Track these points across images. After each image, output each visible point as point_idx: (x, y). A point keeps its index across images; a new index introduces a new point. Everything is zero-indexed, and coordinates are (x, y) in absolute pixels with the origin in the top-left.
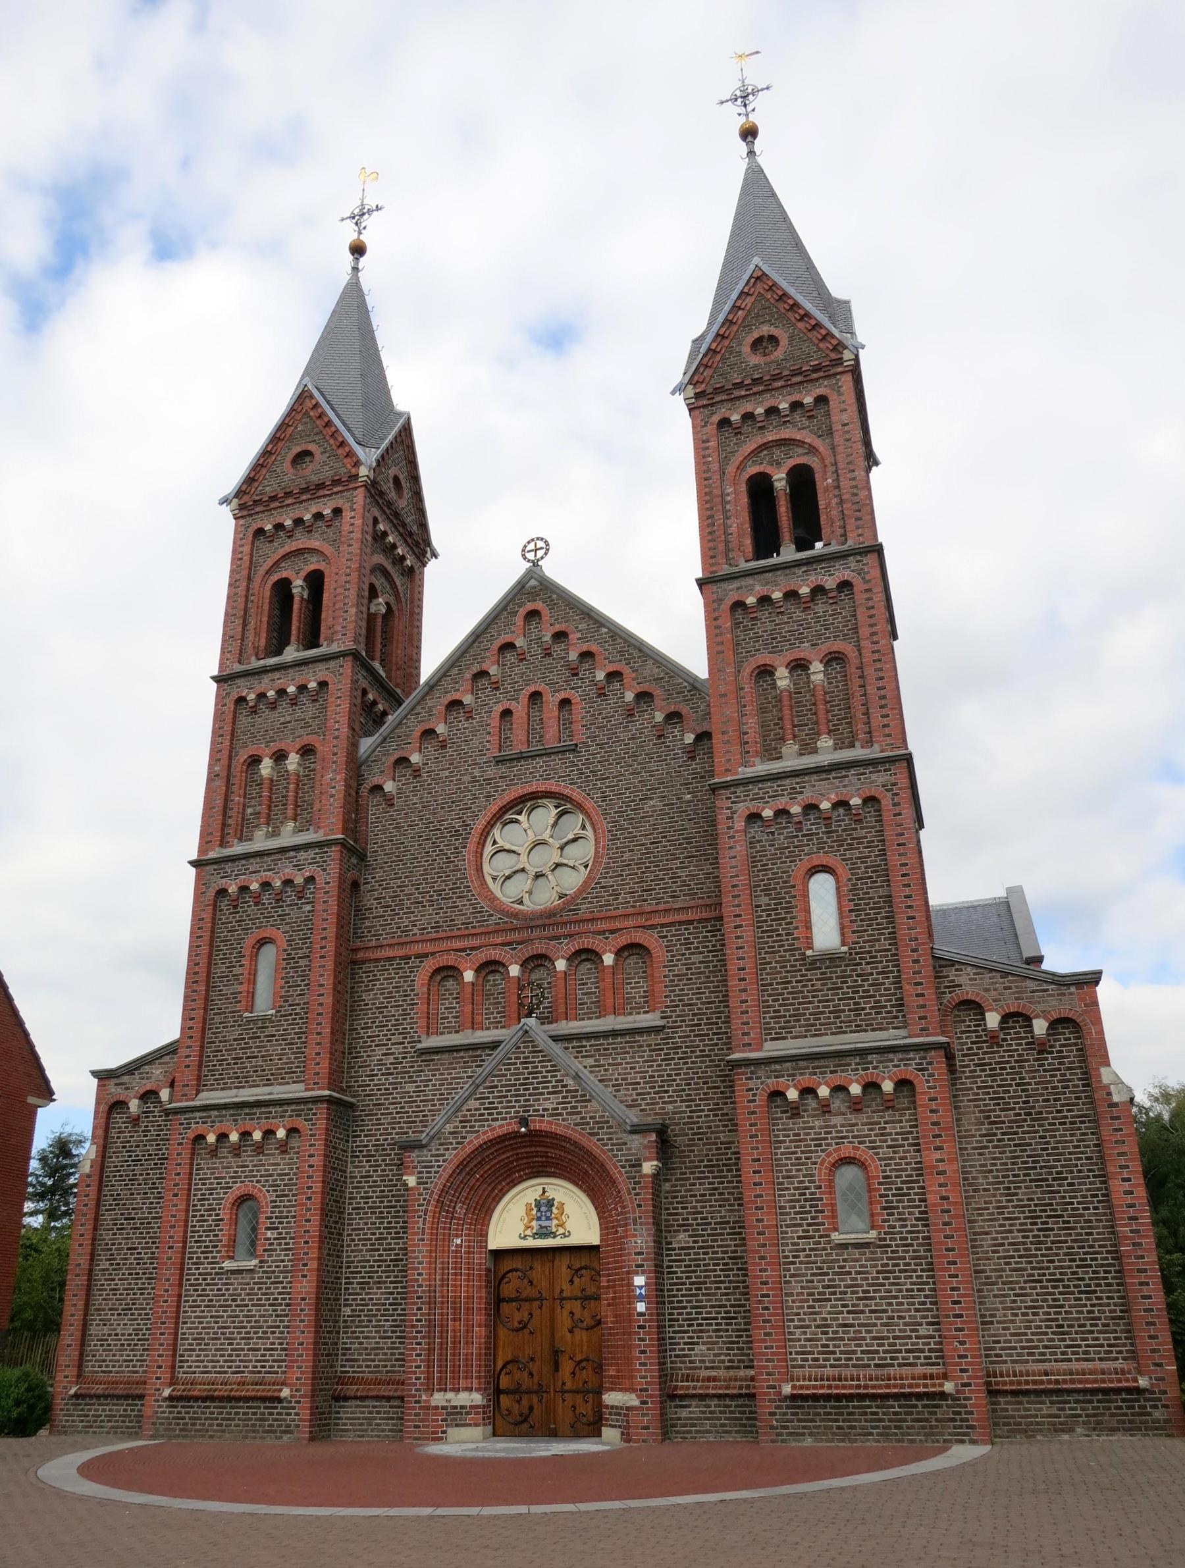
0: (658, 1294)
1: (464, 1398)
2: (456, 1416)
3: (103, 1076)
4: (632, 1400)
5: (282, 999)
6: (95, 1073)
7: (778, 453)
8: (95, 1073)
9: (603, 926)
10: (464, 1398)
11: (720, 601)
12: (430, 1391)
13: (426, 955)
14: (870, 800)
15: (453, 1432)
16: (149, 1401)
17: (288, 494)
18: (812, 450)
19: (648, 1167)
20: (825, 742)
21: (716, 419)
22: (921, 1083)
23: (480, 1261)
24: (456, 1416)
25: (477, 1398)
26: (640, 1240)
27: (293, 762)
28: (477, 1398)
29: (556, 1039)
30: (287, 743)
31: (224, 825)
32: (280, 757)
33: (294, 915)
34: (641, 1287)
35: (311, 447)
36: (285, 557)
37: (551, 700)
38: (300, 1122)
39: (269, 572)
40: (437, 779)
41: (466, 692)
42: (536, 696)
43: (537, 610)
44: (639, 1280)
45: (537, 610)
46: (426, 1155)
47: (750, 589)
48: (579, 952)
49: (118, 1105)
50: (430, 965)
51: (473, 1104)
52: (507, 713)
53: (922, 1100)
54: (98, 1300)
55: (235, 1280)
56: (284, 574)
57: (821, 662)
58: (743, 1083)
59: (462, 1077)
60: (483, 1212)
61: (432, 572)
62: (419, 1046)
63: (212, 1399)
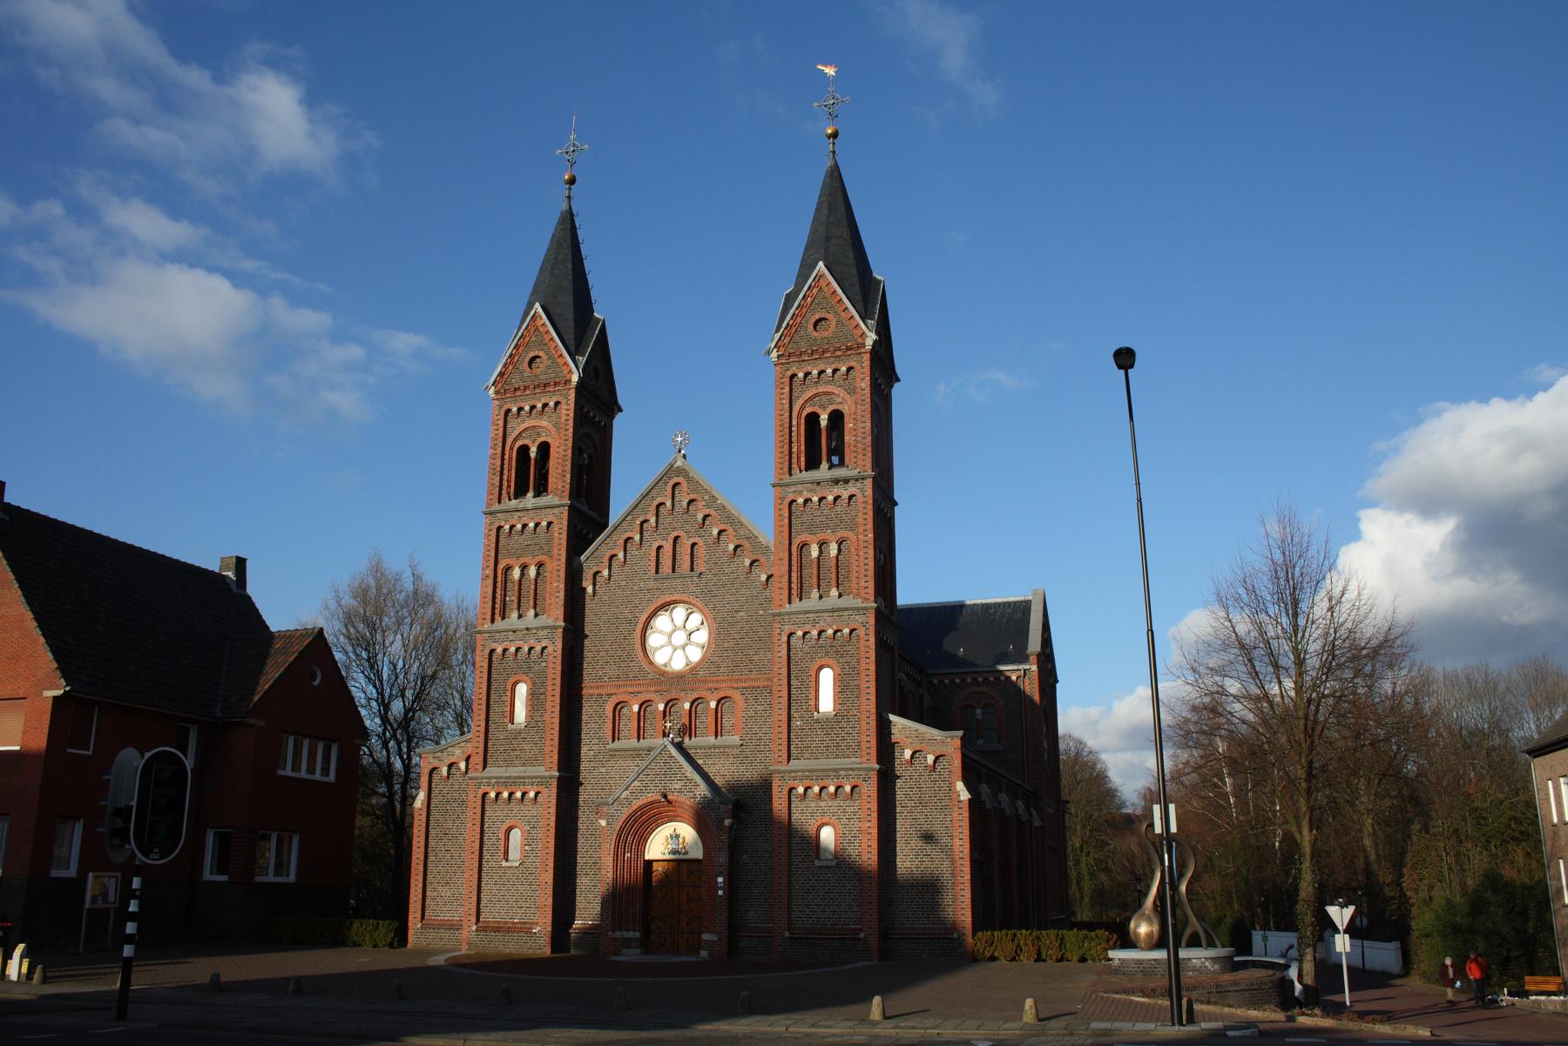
0: (731, 885)
1: (631, 934)
2: (627, 943)
4: (714, 937)
5: (530, 716)
10: (631, 934)
11: (783, 499)
12: (614, 930)
15: (624, 951)
16: (465, 932)
19: (727, 822)
23: (641, 864)
24: (627, 943)
25: (638, 934)
26: (723, 859)
28: (638, 934)
31: (493, 608)
33: (536, 668)
34: (1137, 926)
35: (541, 354)
38: (540, 788)
39: (515, 440)
40: (619, 587)
44: (720, 879)
46: (612, 810)
47: (801, 492)
51: (636, 783)
54: (429, 878)
55: (509, 872)
56: (526, 442)
59: (633, 767)
60: (642, 840)
61: (619, 422)
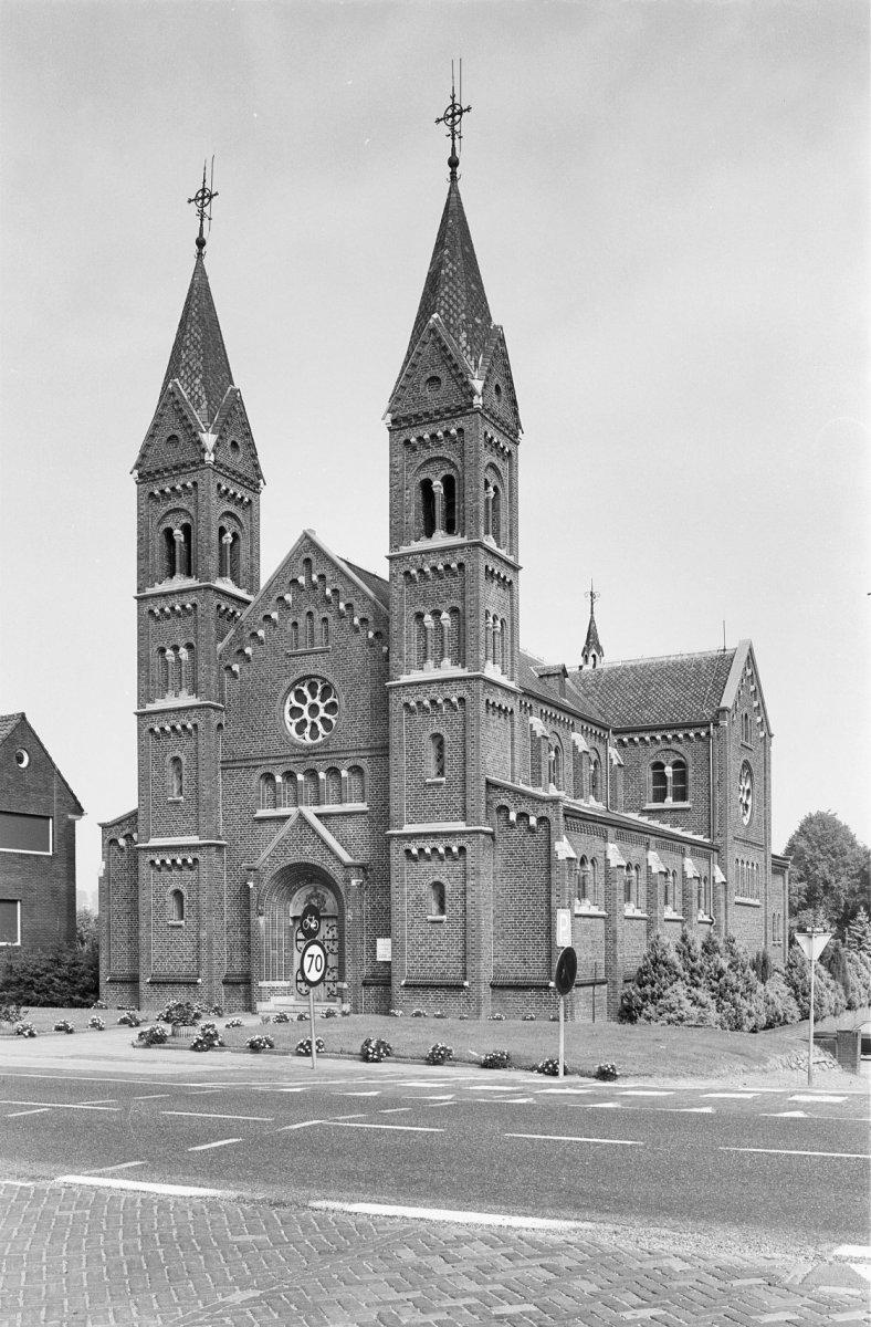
3: (104, 826)
6: (100, 825)
7: (437, 465)
8: (100, 825)
9: (342, 755)
13: (257, 766)
14: (461, 700)
17: (166, 470)
18: (453, 465)
20: (447, 661)
21: (402, 439)
22: (469, 848)
27: (184, 654)
29: (319, 816)
30: (181, 642)
32: (176, 648)
36: (168, 513)
37: (318, 617)
41: (275, 610)
42: (310, 614)
43: (309, 552)
45: (309, 552)
48: (330, 769)
49: (113, 842)
50: (260, 771)
52: (295, 624)
53: (469, 857)
57: (348, 770)
58: (394, 844)
62: (256, 816)
63: (168, 983)
